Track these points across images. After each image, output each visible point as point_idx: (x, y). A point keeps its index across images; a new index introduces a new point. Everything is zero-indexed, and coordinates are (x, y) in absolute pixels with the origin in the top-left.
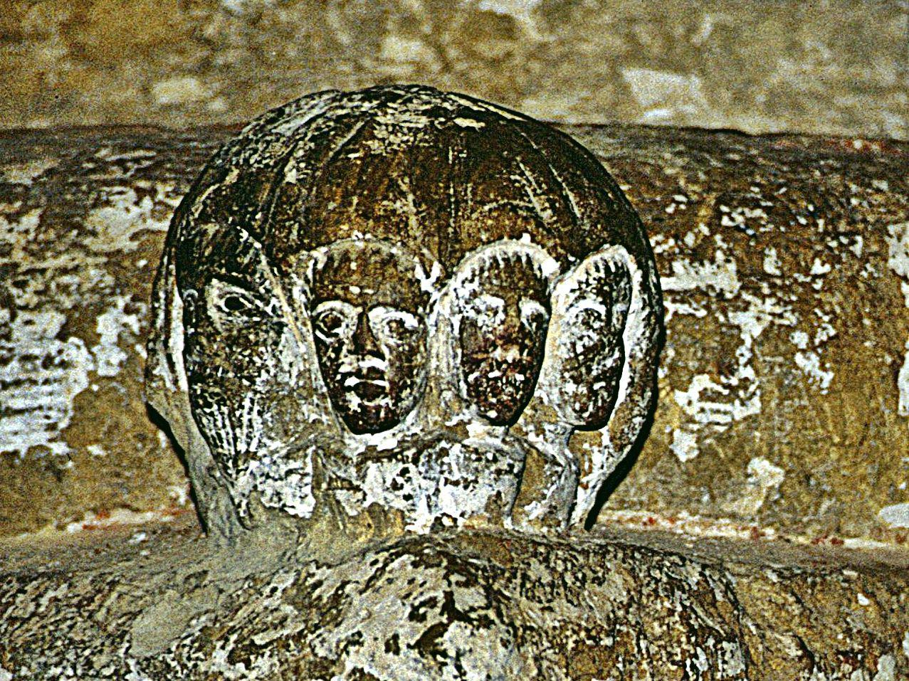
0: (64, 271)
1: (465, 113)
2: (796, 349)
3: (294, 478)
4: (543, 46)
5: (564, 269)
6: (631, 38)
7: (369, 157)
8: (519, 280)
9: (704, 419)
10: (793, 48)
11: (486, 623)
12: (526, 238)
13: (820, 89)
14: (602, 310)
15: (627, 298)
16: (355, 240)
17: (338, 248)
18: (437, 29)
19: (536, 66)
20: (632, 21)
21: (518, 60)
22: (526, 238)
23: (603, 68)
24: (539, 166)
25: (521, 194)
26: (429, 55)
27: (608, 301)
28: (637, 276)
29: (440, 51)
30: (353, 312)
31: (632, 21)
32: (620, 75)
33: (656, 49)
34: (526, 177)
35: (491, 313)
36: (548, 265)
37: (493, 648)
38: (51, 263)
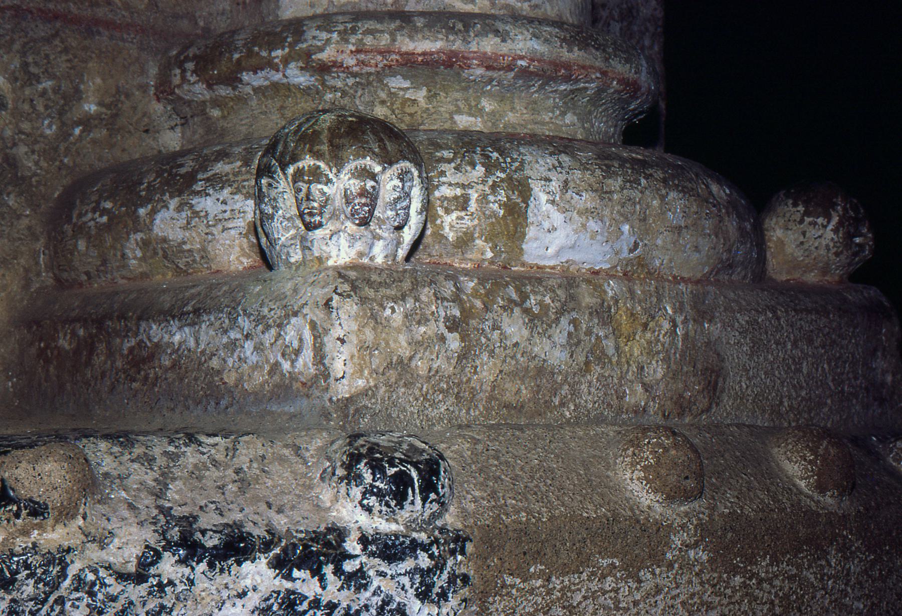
0: (244, 181)
1: (351, 116)
2: (490, 202)
3: (293, 247)
4: (428, 109)
5: (384, 169)
6: (457, 106)
7: (314, 131)
8: (365, 174)
9: (458, 226)
10: (513, 109)
11: (349, 296)
12: (368, 158)
13: (523, 122)
14: (400, 184)
15: (412, 180)
16: (308, 162)
17: (300, 164)
18: (392, 104)
19: (425, 115)
20: (457, 100)
21: (419, 113)
22: (368, 158)
23: (447, 116)
24: (375, 133)
25: (367, 142)
26: (389, 113)
27: (402, 180)
28: (416, 173)
29: (393, 111)
30: (306, 186)
31: (457, 100)
32: (453, 118)
33: (466, 109)
34: (370, 137)
35: (354, 185)
36: (378, 169)
37: (352, 306)
38: (240, 178)
